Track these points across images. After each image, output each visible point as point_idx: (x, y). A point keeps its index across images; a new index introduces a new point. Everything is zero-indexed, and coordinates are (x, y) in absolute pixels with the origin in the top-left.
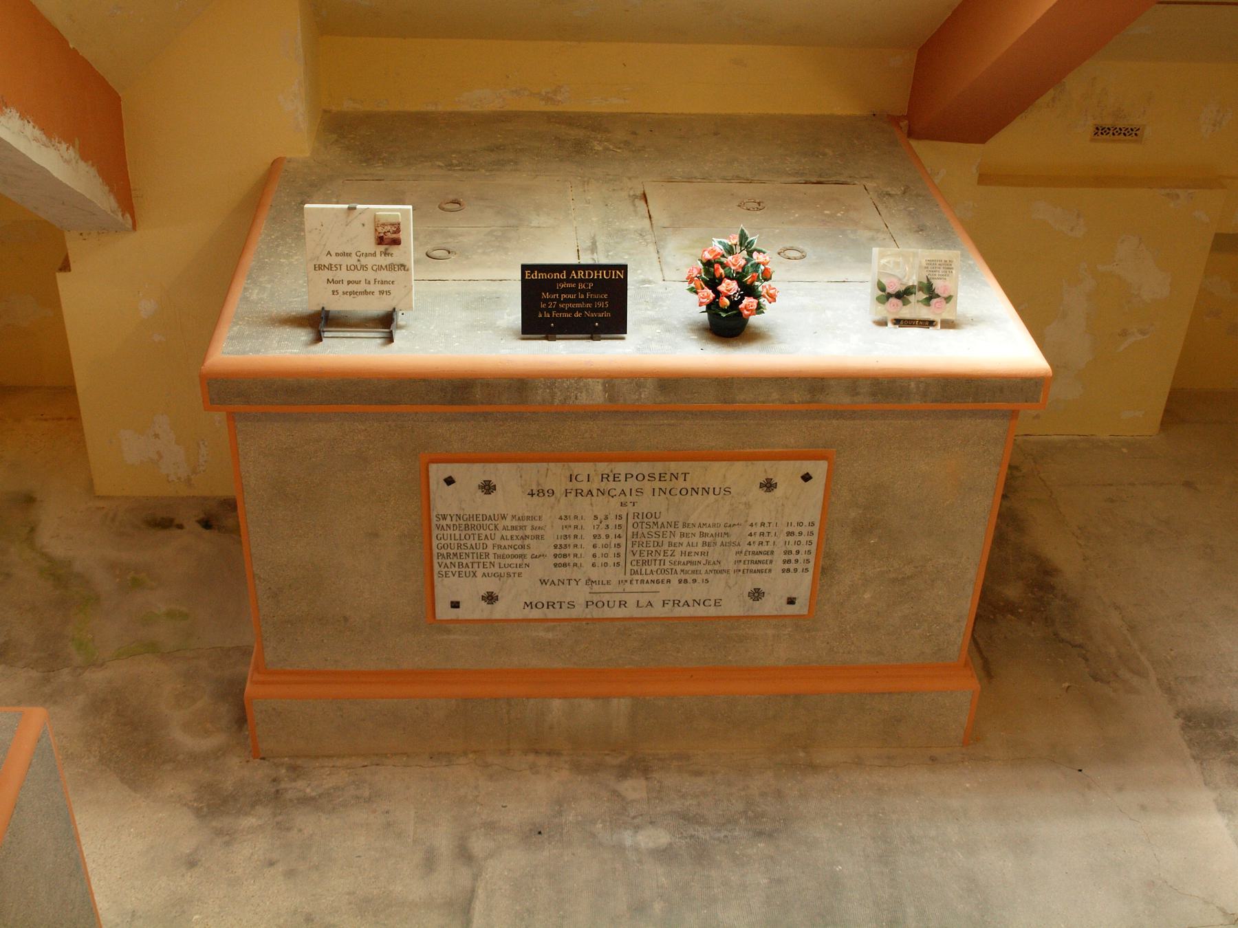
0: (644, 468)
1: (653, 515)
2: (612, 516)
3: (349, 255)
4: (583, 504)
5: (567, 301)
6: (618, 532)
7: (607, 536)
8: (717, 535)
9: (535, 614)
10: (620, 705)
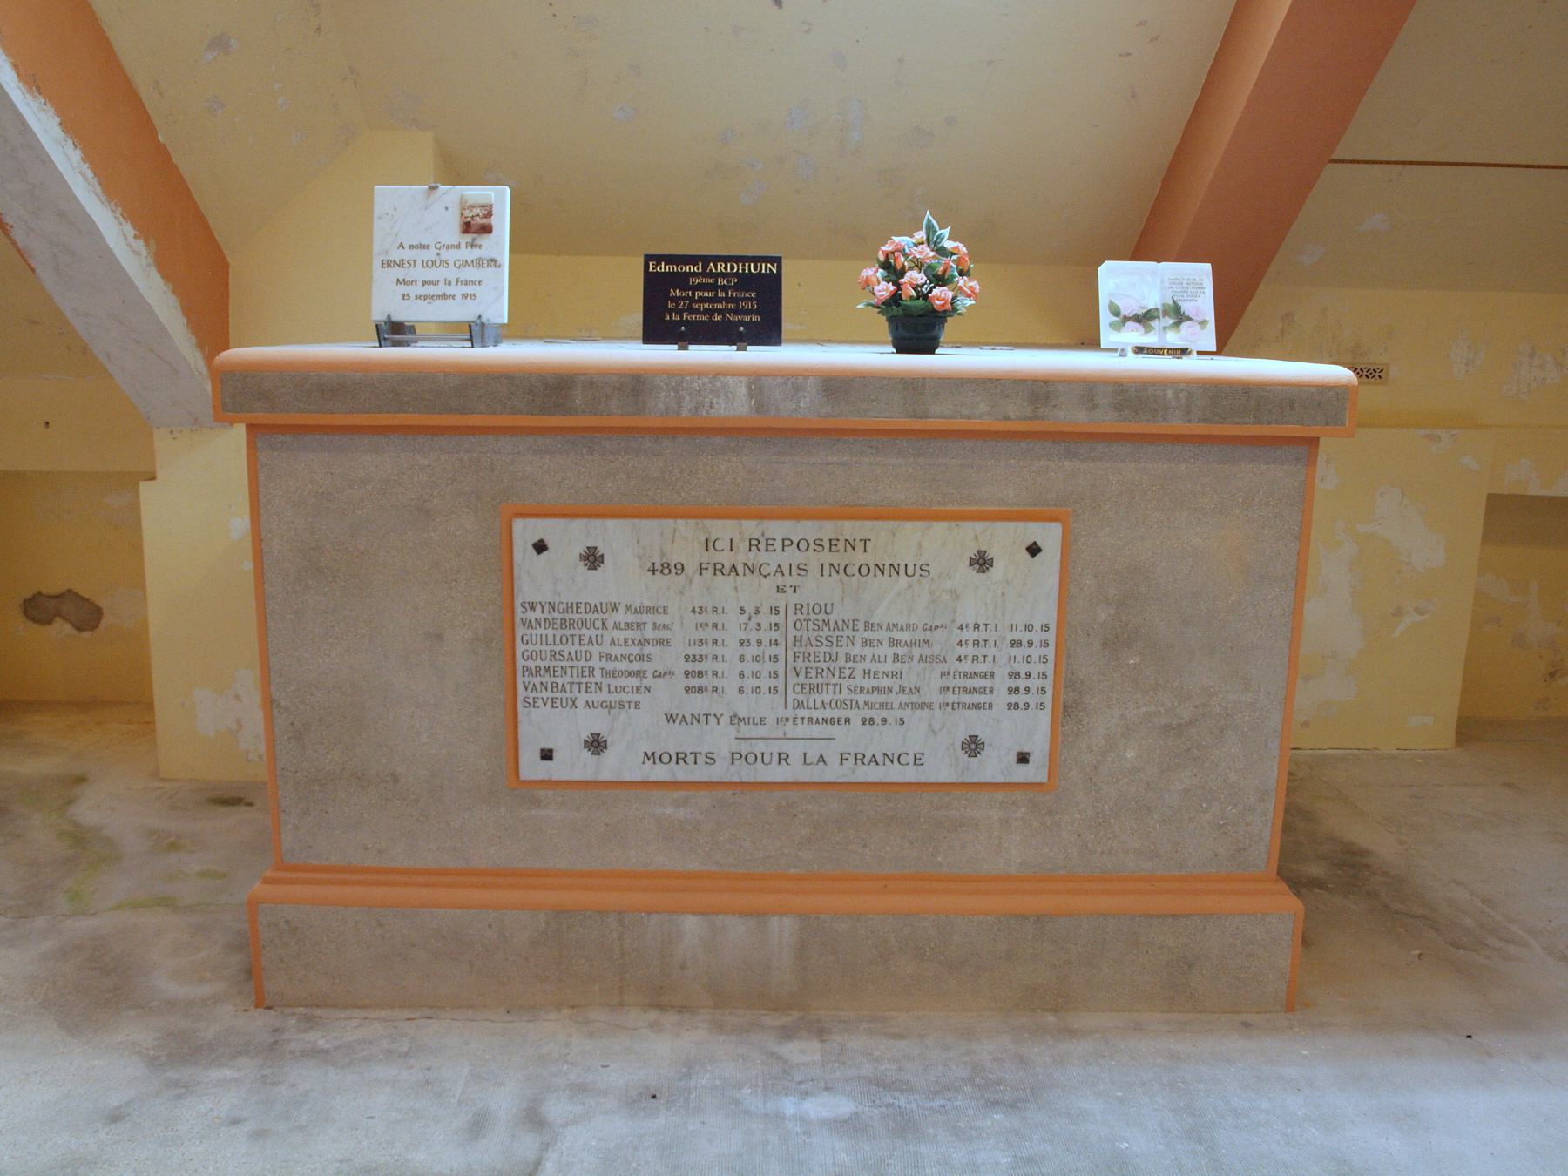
0: (807, 530)
1: (823, 609)
2: (765, 610)
3: (426, 247)
4: (724, 584)
5: (703, 300)
6: (775, 635)
7: (759, 642)
8: (913, 643)
9: (659, 773)
10: (782, 929)
